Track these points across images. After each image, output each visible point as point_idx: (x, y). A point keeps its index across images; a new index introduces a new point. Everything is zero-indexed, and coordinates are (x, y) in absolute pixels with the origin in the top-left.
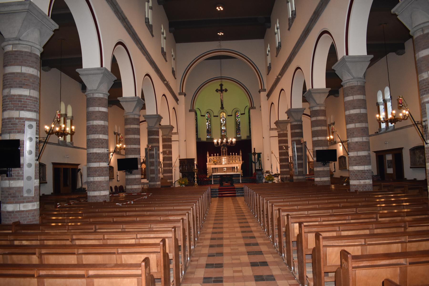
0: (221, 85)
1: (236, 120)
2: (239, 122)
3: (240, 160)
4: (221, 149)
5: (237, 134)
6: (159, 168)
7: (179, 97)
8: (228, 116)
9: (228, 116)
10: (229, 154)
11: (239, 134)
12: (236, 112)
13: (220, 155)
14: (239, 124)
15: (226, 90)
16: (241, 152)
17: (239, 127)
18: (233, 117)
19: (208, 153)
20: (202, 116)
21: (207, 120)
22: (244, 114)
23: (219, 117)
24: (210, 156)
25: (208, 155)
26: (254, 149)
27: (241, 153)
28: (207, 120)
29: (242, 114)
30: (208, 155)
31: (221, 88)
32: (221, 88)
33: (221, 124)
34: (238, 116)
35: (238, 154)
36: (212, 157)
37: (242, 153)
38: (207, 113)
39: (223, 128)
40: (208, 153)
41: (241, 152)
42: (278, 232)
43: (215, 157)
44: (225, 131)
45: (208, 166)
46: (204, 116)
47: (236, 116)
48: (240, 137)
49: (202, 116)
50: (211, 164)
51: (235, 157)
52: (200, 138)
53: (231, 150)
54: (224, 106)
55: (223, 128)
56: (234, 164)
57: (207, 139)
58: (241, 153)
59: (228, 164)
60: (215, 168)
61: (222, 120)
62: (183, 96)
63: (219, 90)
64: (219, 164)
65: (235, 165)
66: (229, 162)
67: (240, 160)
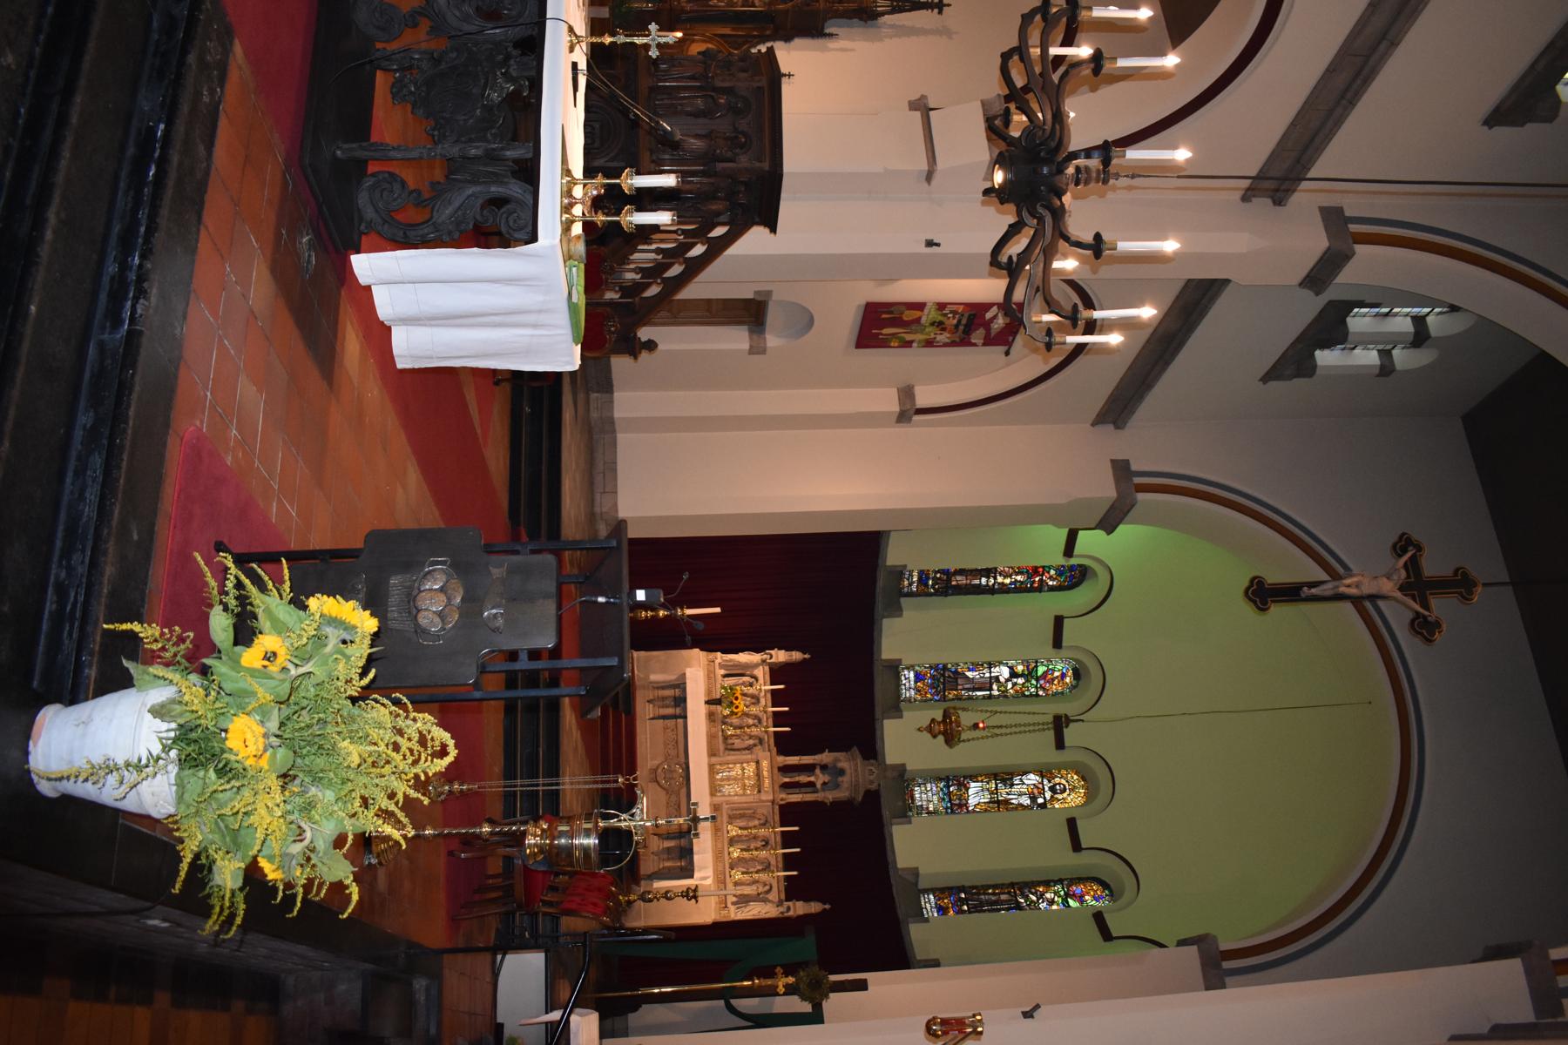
0: (1461, 584)
1: (1047, 884)
2: (1033, 906)
3: (743, 900)
4: (826, 757)
5: (940, 892)
6: (653, 27)
7: (1306, 199)
8: (1072, 824)
9: (1072, 824)
11: (942, 910)
12: (1105, 885)
13: (784, 745)
14: (1019, 907)
17: (994, 906)
18: (1063, 858)
19: (796, 656)
20: (1059, 621)
21: (1030, 674)
22: (1077, 846)
23: (1055, 756)
24: (777, 673)
25: (780, 656)
26: (862, 986)
27: (799, 908)
28: (1030, 674)
29: (1099, 917)
30: (780, 656)
31: (1441, 585)
32: (1441, 585)
34: (1081, 899)
35: (793, 890)
36: (764, 686)
39: (974, 787)
40: (796, 656)
41: (815, 907)
43: (766, 707)
44: (957, 805)
45: (705, 913)
46: (1057, 643)
47: (1070, 881)
48: (919, 915)
49: (1059, 621)
50: (710, 675)
51: (767, 868)
52: (897, 611)
54: (1277, 611)
55: (974, 787)
56: (718, 855)
57: (894, 668)
58: (799, 908)
60: (681, 701)
61: (1032, 779)
63: (1413, 566)
64: (711, 738)
65: (704, 874)
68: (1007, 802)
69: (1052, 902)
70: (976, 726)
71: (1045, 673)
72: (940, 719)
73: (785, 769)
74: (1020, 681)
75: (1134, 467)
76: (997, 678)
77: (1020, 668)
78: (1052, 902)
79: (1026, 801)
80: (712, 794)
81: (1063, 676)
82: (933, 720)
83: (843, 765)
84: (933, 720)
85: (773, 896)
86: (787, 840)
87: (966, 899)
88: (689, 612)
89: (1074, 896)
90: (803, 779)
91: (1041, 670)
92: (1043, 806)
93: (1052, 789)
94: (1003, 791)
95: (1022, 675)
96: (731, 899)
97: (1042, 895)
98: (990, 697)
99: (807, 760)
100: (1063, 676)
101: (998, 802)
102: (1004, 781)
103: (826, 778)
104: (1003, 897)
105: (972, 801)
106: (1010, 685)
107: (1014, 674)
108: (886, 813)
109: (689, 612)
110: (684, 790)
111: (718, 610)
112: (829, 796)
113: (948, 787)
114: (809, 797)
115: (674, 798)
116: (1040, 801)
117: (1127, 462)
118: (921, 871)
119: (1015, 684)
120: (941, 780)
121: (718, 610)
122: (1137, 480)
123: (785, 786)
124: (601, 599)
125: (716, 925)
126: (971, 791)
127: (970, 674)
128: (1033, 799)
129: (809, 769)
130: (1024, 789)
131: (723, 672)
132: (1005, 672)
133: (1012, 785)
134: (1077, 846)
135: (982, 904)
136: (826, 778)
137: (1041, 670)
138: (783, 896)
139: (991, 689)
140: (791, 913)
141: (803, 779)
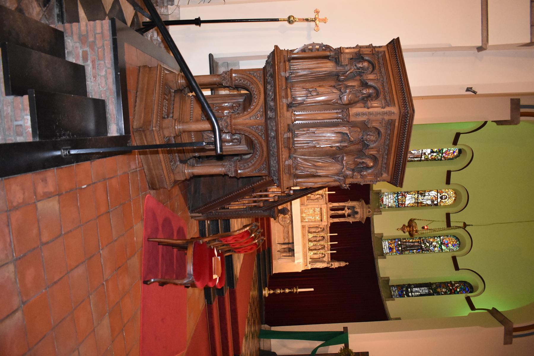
4: (350, 204)
9: (448, 215)
10: (333, 227)
15: (324, 21)
16: (343, 264)
21: (440, 151)
22: (457, 268)
28: (440, 151)
33: (423, 194)
34: (447, 245)
35: (334, 257)
37: (339, 268)
38: (460, 151)
41: (343, 264)
42: (137, 146)
48: (383, 255)
53: (353, 241)
55: (408, 196)
58: (336, 265)
59: (303, 227)
61: (433, 193)
62: (480, 44)
66: (308, 229)
67: (314, 261)
68: (421, 203)
69: (435, 247)
70: (423, 228)
71: (446, 151)
72: (407, 225)
73: (332, 210)
74: (435, 154)
75: (522, 103)
76: (425, 154)
77: (435, 150)
78: (435, 247)
79: (429, 202)
80: (302, 221)
81: (454, 152)
82: (404, 225)
83: (358, 210)
84: (404, 225)
85: (326, 259)
86: (332, 239)
87: (401, 244)
88: (299, 290)
89: (444, 244)
90: (340, 212)
91: (445, 150)
92: (437, 205)
93: (441, 198)
94: (420, 198)
95: (436, 152)
96: (309, 260)
97: (432, 243)
98: (420, 161)
99: (342, 204)
100: (454, 152)
101: (418, 203)
102: (421, 194)
103: (350, 211)
104: (416, 244)
105: (407, 202)
106: (430, 156)
107: (432, 152)
108: (375, 256)
109: (299, 290)
110: (291, 226)
111: (312, 289)
112: (351, 220)
113: (398, 196)
114: (342, 220)
115: (286, 229)
116: (436, 202)
117: (519, 100)
118: (391, 279)
119: (432, 156)
120: (395, 193)
121: (312, 289)
122: (522, 110)
123: (332, 217)
124: (253, 235)
125: (305, 272)
126: (407, 198)
127: (413, 152)
128: (433, 201)
129: (343, 209)
130: (429, 197)
131: (310, 260)
132: (429, 151)
133: (425, 196)
134: (457, 268)
135: (407, 247)
136: (350, 211)
137: (445, 150)
138: (330, 260)
139: (421, 157)
140: (333, 267)
141: (340, 212)
